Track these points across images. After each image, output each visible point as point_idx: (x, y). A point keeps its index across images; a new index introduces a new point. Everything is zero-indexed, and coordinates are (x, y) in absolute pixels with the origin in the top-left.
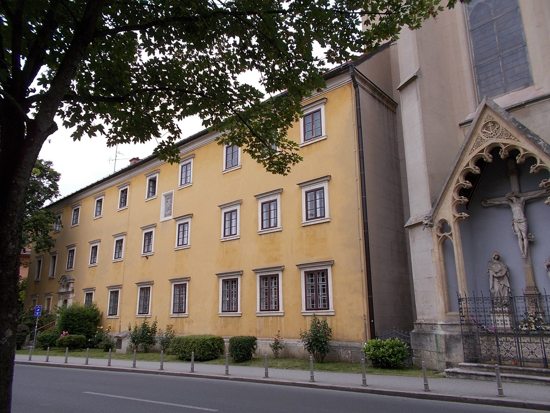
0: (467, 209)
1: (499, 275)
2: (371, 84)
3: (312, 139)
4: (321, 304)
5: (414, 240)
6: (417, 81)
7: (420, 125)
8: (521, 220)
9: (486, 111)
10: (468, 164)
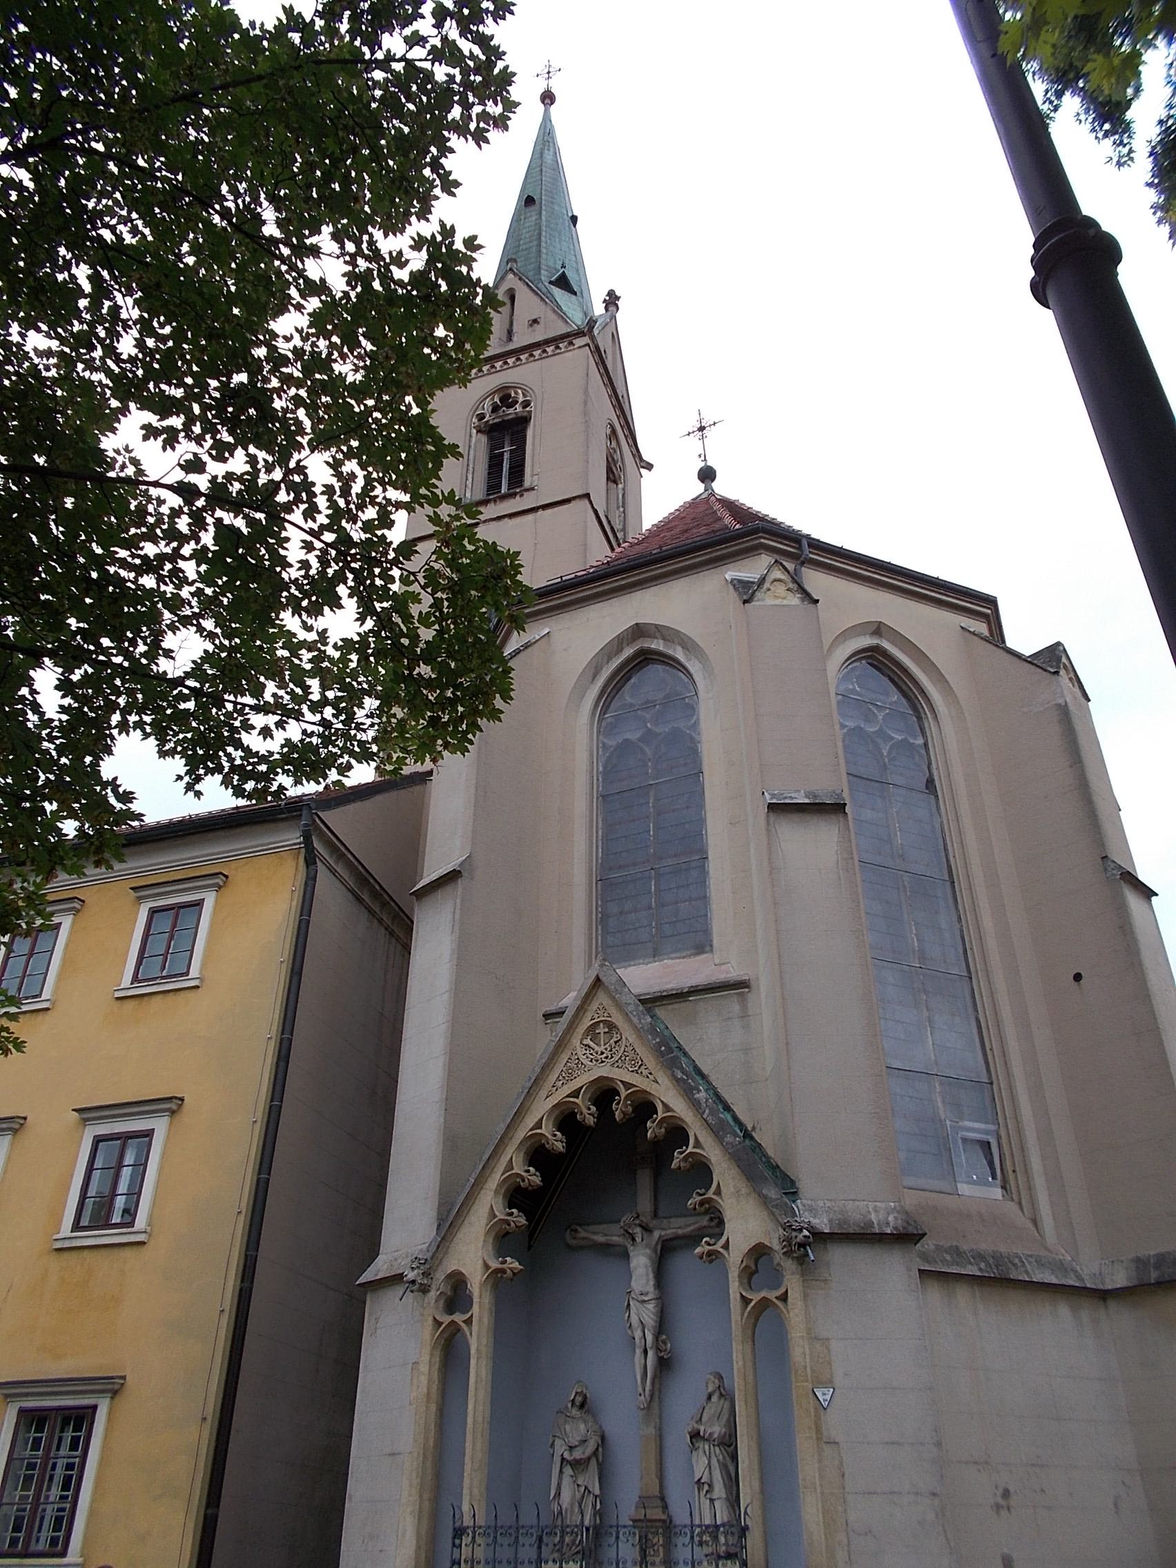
0: (529, 1248)
1: (578, 1454)
2: (356, 863)
3: (158, 981)
4: (44, 1534)
5: (376, 1328)
6: (460, 885)
7: (446, 996)
8: (647, 1294)
9: (598, 993)
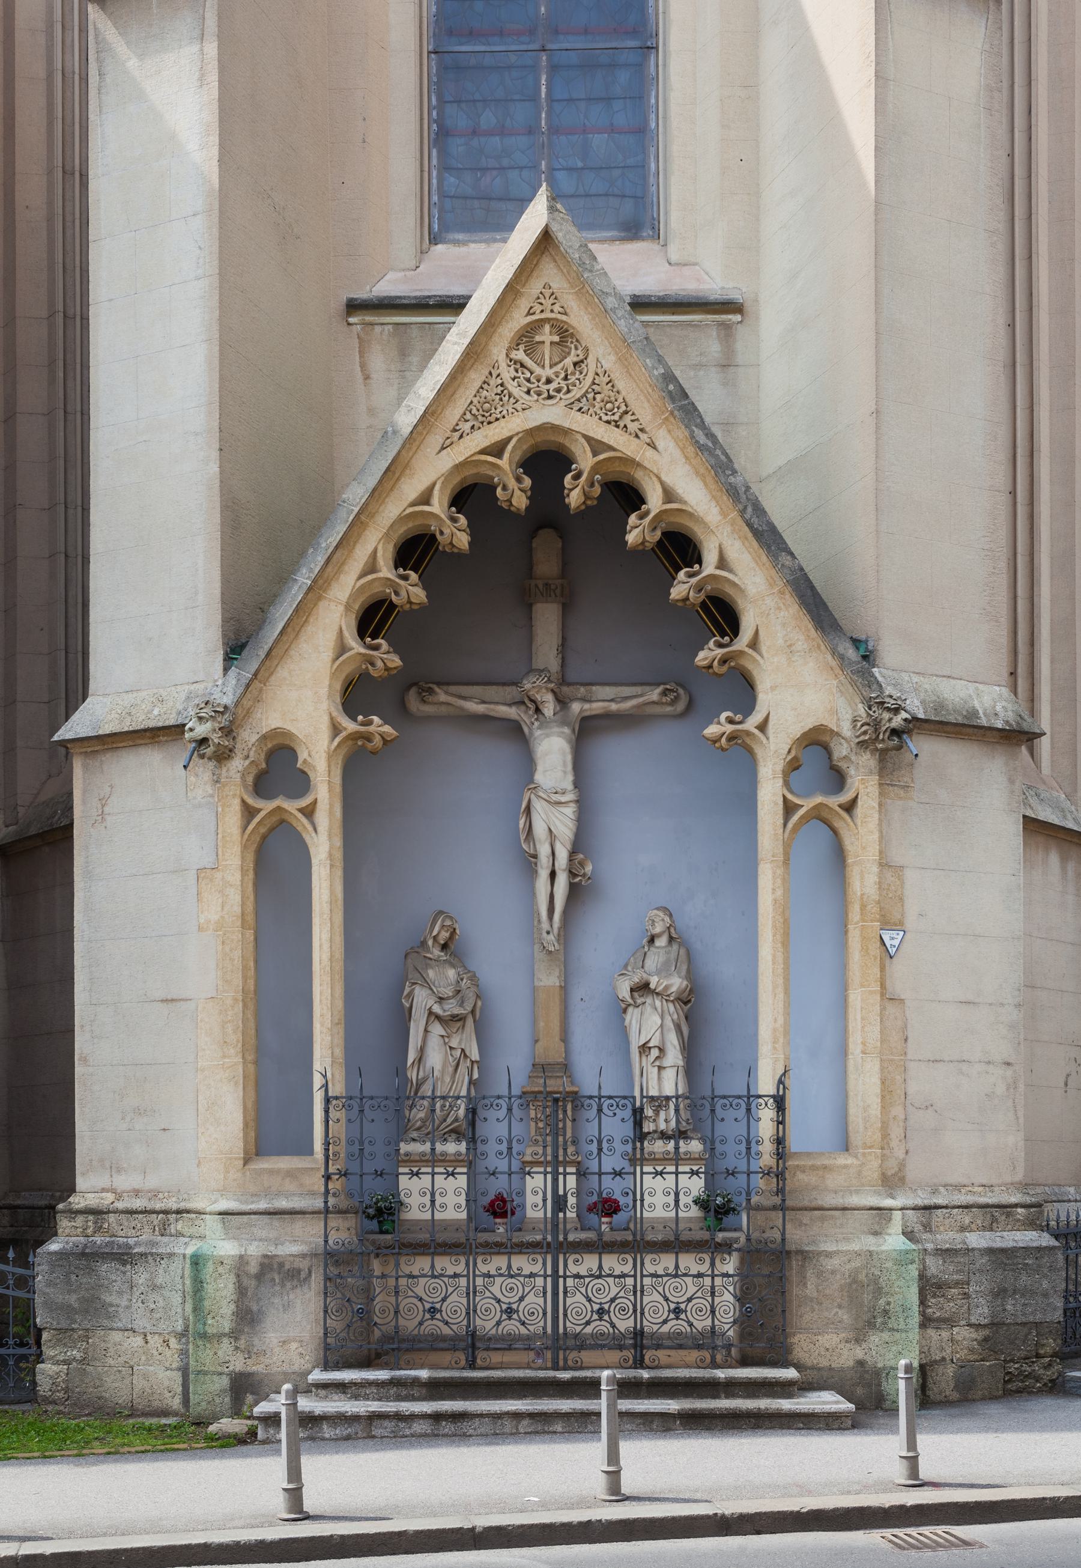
1: (452, 1008)
10: (430, 490)
